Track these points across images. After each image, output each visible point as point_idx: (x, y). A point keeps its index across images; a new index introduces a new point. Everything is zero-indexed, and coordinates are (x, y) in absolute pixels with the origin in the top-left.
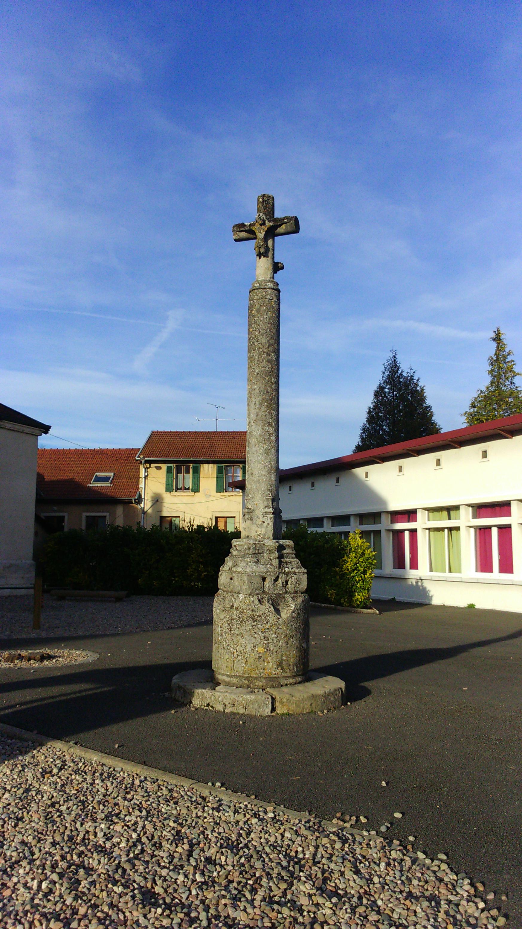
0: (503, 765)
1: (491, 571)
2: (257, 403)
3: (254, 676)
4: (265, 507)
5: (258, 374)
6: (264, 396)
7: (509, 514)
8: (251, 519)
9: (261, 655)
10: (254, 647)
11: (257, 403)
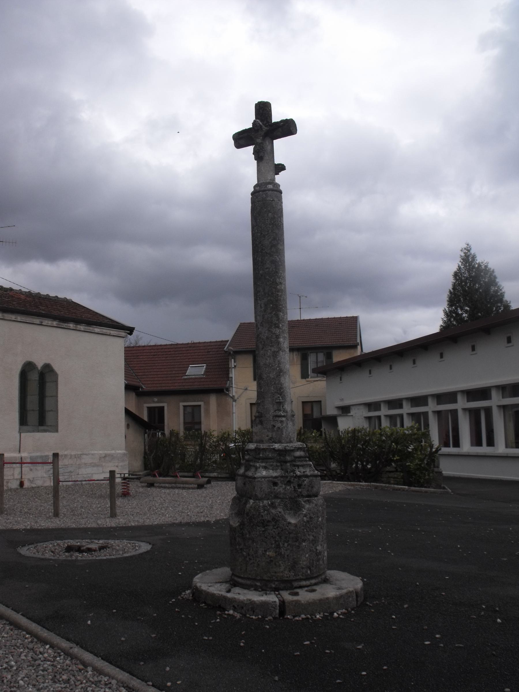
2: (263, 305)
3: (266, 579)
4: (275, 411)
5: (262, 275)
8: (261, 423)
10: (265, 551)
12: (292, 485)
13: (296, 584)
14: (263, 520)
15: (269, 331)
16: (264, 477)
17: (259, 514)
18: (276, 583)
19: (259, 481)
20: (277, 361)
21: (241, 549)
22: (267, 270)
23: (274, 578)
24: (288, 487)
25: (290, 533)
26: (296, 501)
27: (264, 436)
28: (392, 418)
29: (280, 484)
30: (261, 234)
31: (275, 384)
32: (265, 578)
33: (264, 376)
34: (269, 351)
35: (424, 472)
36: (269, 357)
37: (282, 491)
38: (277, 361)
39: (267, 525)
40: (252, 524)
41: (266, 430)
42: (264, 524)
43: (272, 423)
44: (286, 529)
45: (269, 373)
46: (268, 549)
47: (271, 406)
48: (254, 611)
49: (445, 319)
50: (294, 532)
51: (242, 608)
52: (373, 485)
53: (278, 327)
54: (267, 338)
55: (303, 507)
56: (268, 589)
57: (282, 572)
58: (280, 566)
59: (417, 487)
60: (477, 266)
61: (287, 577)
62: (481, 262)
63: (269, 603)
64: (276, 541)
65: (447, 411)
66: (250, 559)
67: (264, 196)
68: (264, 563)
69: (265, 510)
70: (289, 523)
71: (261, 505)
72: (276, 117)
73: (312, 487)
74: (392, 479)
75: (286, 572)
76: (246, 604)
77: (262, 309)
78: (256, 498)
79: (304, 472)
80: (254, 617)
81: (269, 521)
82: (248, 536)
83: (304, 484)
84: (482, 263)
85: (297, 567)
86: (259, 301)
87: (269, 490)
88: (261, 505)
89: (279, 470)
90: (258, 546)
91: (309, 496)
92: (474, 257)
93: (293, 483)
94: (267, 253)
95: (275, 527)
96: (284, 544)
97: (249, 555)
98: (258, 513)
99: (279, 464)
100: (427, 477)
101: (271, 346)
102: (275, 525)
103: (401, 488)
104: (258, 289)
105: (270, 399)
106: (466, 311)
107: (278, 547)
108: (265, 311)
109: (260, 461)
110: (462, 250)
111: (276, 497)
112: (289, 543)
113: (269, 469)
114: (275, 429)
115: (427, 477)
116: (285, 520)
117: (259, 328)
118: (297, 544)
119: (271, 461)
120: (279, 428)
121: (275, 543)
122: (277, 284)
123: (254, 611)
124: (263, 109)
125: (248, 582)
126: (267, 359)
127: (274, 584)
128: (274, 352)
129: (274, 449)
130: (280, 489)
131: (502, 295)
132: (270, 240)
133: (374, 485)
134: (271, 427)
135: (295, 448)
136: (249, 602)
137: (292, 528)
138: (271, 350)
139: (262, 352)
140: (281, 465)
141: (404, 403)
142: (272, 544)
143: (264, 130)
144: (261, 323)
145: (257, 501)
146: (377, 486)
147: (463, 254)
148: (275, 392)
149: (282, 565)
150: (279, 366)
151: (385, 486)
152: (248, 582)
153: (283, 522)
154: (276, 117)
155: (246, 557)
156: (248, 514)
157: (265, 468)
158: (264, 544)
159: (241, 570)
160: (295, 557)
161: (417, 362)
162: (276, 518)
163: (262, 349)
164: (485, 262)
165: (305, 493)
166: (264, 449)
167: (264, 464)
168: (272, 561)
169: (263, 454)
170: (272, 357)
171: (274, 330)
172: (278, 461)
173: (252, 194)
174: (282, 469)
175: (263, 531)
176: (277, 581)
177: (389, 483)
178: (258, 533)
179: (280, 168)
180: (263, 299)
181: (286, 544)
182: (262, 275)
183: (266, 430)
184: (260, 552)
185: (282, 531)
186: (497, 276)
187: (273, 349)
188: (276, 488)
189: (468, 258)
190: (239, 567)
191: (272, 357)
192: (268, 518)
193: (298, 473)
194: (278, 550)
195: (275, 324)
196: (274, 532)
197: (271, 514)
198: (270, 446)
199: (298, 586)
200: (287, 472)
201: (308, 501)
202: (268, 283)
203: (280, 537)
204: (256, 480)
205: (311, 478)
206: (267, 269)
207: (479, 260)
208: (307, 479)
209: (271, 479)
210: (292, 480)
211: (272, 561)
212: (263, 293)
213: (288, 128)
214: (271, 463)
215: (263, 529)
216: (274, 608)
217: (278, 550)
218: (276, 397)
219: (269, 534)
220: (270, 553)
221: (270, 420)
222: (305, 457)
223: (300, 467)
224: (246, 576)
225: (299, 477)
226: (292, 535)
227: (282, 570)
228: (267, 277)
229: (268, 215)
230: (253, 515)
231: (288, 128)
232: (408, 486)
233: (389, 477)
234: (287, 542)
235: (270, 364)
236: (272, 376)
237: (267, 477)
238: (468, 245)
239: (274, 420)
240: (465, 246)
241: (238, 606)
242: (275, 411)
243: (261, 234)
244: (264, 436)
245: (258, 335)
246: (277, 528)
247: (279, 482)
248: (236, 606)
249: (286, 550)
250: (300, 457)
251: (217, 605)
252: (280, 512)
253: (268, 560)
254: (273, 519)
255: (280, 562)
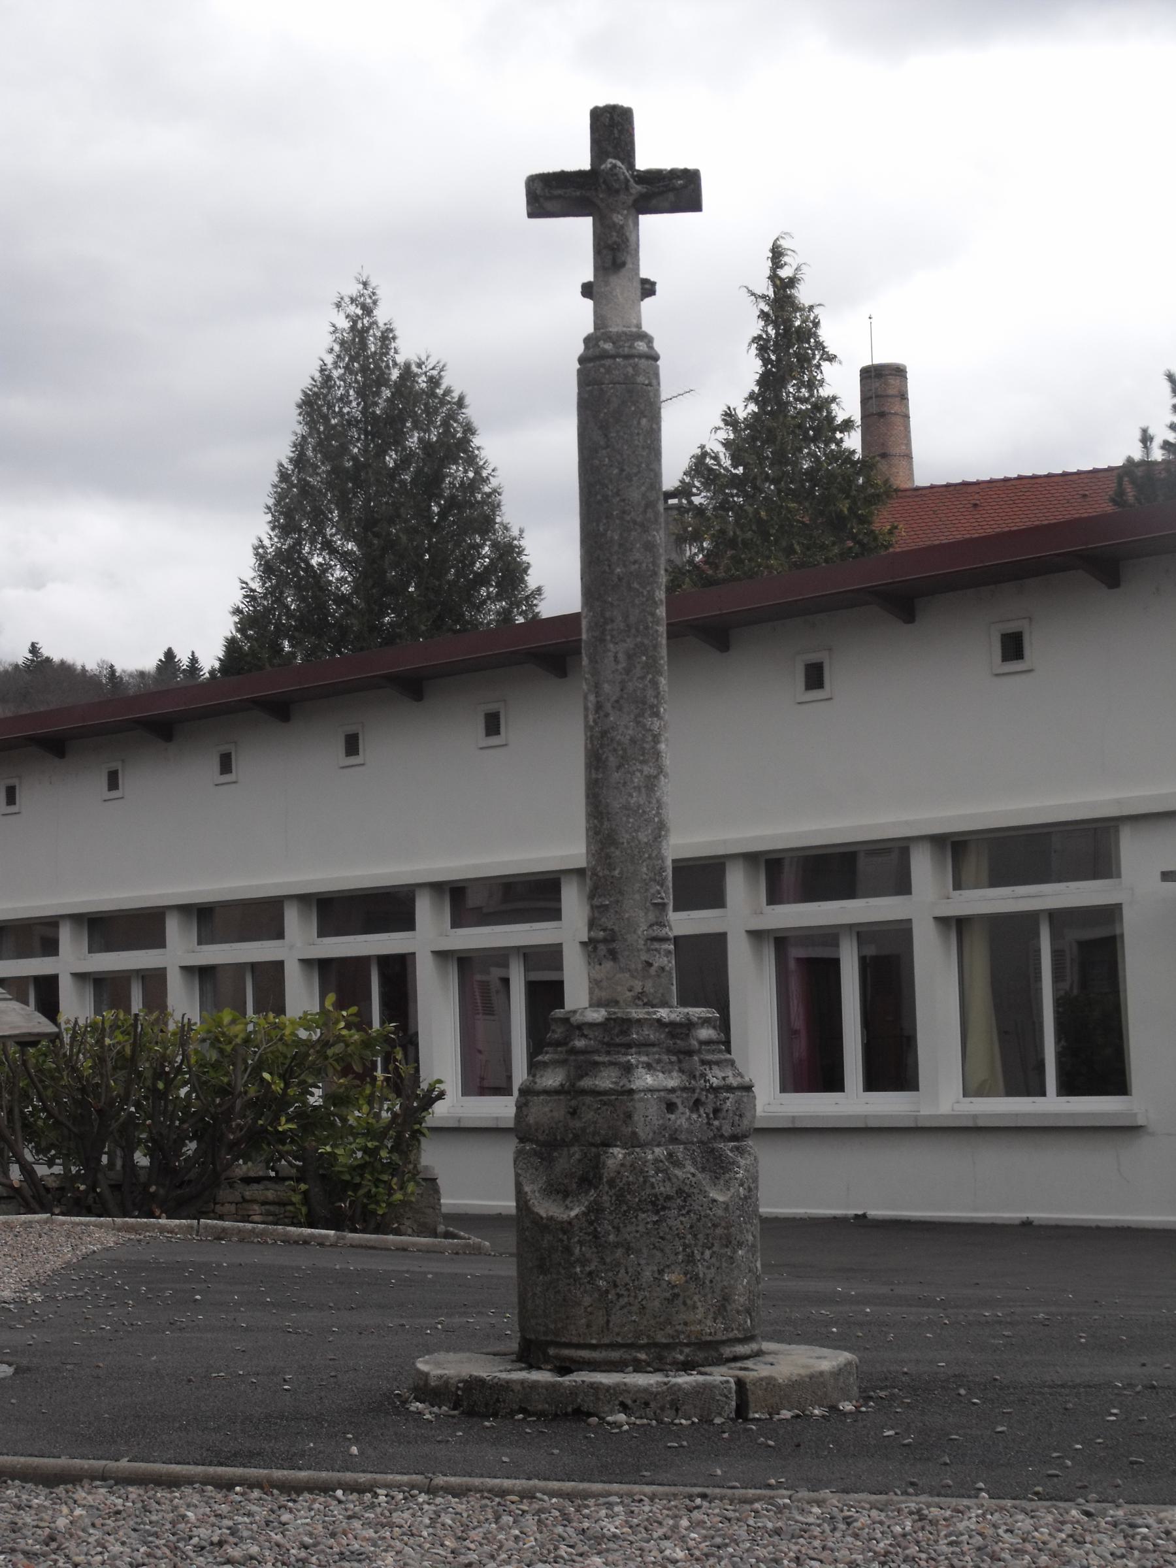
0: (665, 1512)
1: (1043, 1094)
2: (621, 656)
3: (664, 1341)
4: (651, 926)
5: (620, 579)
6: (639, 639)
7: (554, 914)
8: (613, 955)
9: (676, 1291)
10: (661, 1272)
11: (621, 656)
12: (702, 1111)
13: (727, 1351)
14: (656, 1196)
15: (638, 723)
16: (651, 1090)
17: (645, 1182)
18: (687, 1350)
19: (641, 1100)
20: (654, 801)
21: (590, 1273)
22: (637, 566)
23: (682, 1337)
24: (694, 1116)
25: (715, 1226)
26: (713, 1150)
27: (619, 989)
28: (108, 989)
29: (681, 1108)
30: (622, 470)
31: (650, 857)
32: (661, 1338)
33: (624, 837)
34: (638, 774)
35: (385, 1177)
36: (638, 789)
37: (685, 1125)
38: (654, 801)
39: (664, 1208)
40: (625, 1208)
41: (627, 975)
42: (657, 1205)
43: (644, 957)
44: (707, 1216)
45: (636, 831)
46: (668, 1266)
47: (642, 914)
48: (677, 1410)
49: (256, 585)
50: (723, 1224)
51: (647, 1404)
52: (206, 1226)
53: (657, 715)
54: (633, 741)
55: (733, 1163)
56: (668, 1367)
57: (700, 1322)
58: (695, 1307)
59: (363, 1231)
60: (395, 374)
61: (710, 1334)
62: (414, 359)
63: (714, 1387)
64: (685, 1246)
65: (239, 968)
66: (619, 1296)
67: (630, 370)
68: (657, 1303)
69: (658, 1171)
70: (714, 1201)
71: (650, 1157)
72: (647, 158)
73: (740, 1116)
74: (256, 1207)
75: (709, 1323)
76: (658, 1393)
77: (620, 667)
78: (633, 1142)
79: (724, 1078)
80: (683, 1421)
81: (668, 1198)
82: (612, 1238)
83: (725, 1107)
84: (419, 366)
85: (729, 1308)
86: (611, 646)
87: (661, 1122)
88: (650, 1157)
89: (675, 1074)
90: (643, 1262)
91: (734, 1138)
92: (387, 337)
93: (703, 1104)
94: (635, 522)
95: (684, 1212)
96: (702, 1254)
97: (616, 1286)
98: (641, 1179)
99: (674, 1058)
100: (398, 1196)
101: (642, 762)
102: (683, 1207)
103: (312, 1236)
104: (608, 614)
105: (637, 897)
106: (345, 559)
107: (690, 1259)
108: (628, 671)
109: (633, 1050)
110: (338, 305)
111: (674, 1140)
112: (715, 1249)
113: (655, 1070)
114: (653, 971)
115: (398, 1196)
116: (705, 1194)
117: (607, 715)
118: (729, 1252)
119: (655, 1049)
120: (663, 969)
121: (684, 1250)
122: (655, 603)
123: (677, 1410)
124: (612, 128)
125: (615, 1355)
126: (631, 795)
127: (681, 1353)
128: (649, 777)
129: (659, 1021)
130: (682, 1119)
131: (491, 504)
132: (643, 488)
133: (214, 1227)
134: (640, 966)
135: (699, 1018)
136: (665, 1387)
137: (720, 1213)
138: (641, 771)
139: (616, 775)
140: (680, 1061)
141: (65, 935)
142: (677, 1254)
143: (633, 191)
144: (617, 701)
145: (637, 1150)
146: (224, 1230)
147: (345, 324)
148: (651, 880)
149: (699, 1304)
150: (658, 814)
151: (253, 1231)
152: (615, 1355)
153: (701, 1197)
154: (647, 158)
155: (607, 1292)
156: (611, 1183)
157: (649, 1067)
158: (658, 1254)
159: (588, 1326)
160: (725, 1283)
161: (241, 764)
162: (686, 1189)
163: (619, 768)
164: (431, 363)
165: (727, 1130)
166: (639, 1020)
167: (644, 1059)
168: (676, 1296)
169: (637, 1034)
170: (643, 790)
171: (648, 721)
172: (669, 1051)
173: (582, 360)
174: (681, 1071)
175: (655, 1223)
176: (687, 1345)
177: (246, 1219)
178: (641, 1228)
179: (648, 289)
180: (625, 641)
181: (708, 1253)
182: (620, 579)
183: (627, 975)
184: (647, 1274)
185: (699, 1220)
186: (476, 423)
187: (647, 770)
188: (673, 1117)
189: (363, 347)
190: (583, 1321)
191: (643, 790)
192: (666, 1189)
193: (715, 1082)
194: (689, 1268)
195: (652, 707)
196: (682, 1223)
197: (674, 1180)
198: (648, 1013)
199: (731, 1356)
200: (694, 1077)
201: (737, 1148)
202: (637, 601)
203: (695, 1236)
204: (636, 1097)
205: (738, 1093)
206: (635, 562)
207: (406, 350)
208: (732, 1096)
209: (662, 1093)
210: (703, 1098)
211: (676, 1296)
212: (622, 626)
213: (679, 191)
214: (657, 1056)
215: (655, 1218)
216: (726, 1397)
217: (689, 1268)
218: (652, 891)
219: (670, 1228)
220: (673, 1277)
221: (638, 951)
222: (718, 1042)
223: (715, 1067)
224: (606, 1341)
225: (715, 1090)
226: (719, 1231)
227: (699, 1317)
228: (636, 585)
229: (639, 423)
230: (628, 1184)
231: (679, 191)
232: (337, 1229)
233: (245, 1200)
234: (709, 1248)
235: (639, 806)
236: (643, 837)
237: (659, 1091)
238: (365, 284)
239: (648, 950)
240: (354, 289)
241: (635, 1401)
242: (651, 926)
243: (622, 470)
244: (619, 989)
245: (604, 733)
246: (688, 1212)
247: (678, 1101)
248: (629, 1402)
249: (709, 1268)
250: (709, 1042)
251: (569, 1409)
252: (693, 1175)
253: (668, 1295)
254: (680, 1192)
255: (696, 1298)
